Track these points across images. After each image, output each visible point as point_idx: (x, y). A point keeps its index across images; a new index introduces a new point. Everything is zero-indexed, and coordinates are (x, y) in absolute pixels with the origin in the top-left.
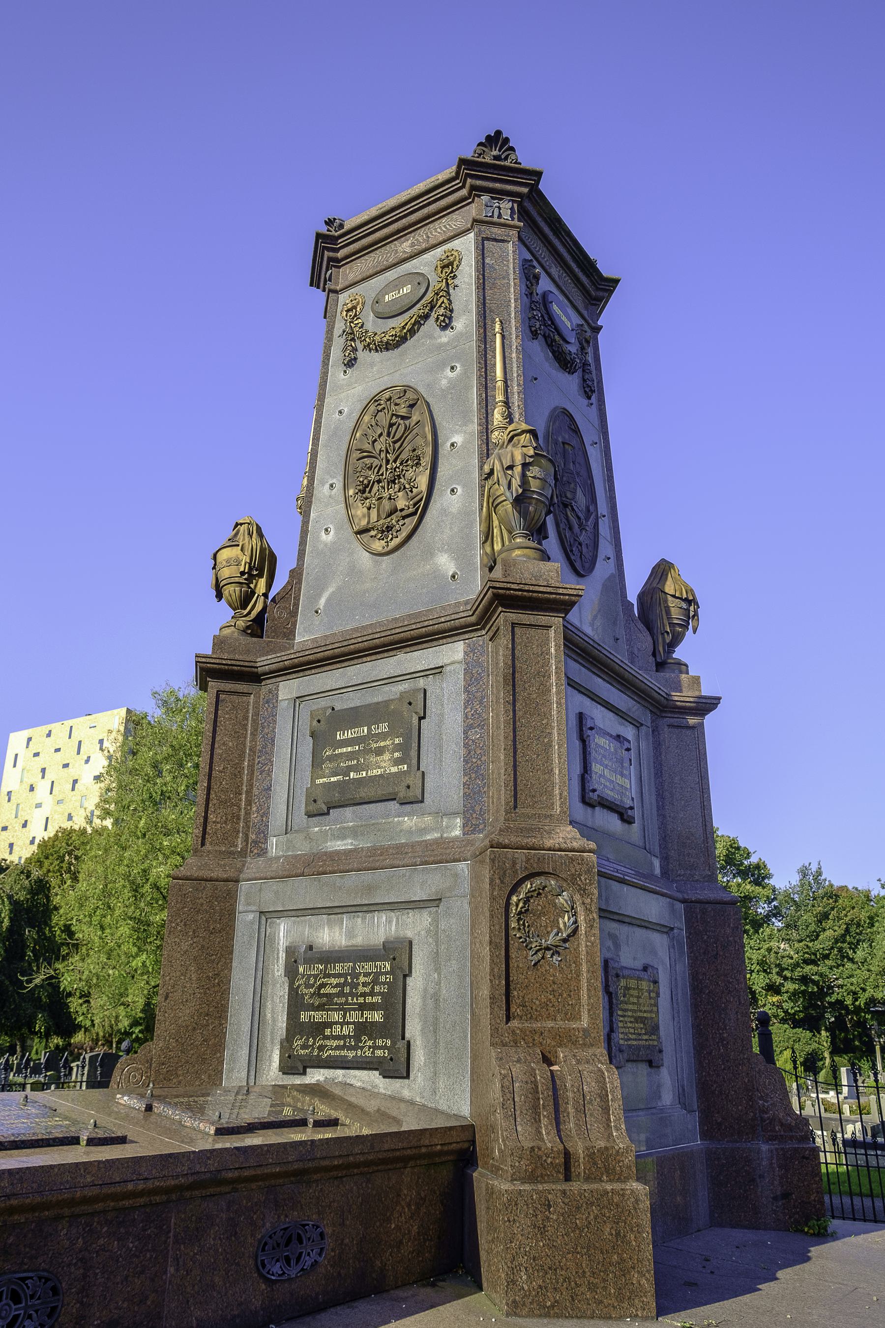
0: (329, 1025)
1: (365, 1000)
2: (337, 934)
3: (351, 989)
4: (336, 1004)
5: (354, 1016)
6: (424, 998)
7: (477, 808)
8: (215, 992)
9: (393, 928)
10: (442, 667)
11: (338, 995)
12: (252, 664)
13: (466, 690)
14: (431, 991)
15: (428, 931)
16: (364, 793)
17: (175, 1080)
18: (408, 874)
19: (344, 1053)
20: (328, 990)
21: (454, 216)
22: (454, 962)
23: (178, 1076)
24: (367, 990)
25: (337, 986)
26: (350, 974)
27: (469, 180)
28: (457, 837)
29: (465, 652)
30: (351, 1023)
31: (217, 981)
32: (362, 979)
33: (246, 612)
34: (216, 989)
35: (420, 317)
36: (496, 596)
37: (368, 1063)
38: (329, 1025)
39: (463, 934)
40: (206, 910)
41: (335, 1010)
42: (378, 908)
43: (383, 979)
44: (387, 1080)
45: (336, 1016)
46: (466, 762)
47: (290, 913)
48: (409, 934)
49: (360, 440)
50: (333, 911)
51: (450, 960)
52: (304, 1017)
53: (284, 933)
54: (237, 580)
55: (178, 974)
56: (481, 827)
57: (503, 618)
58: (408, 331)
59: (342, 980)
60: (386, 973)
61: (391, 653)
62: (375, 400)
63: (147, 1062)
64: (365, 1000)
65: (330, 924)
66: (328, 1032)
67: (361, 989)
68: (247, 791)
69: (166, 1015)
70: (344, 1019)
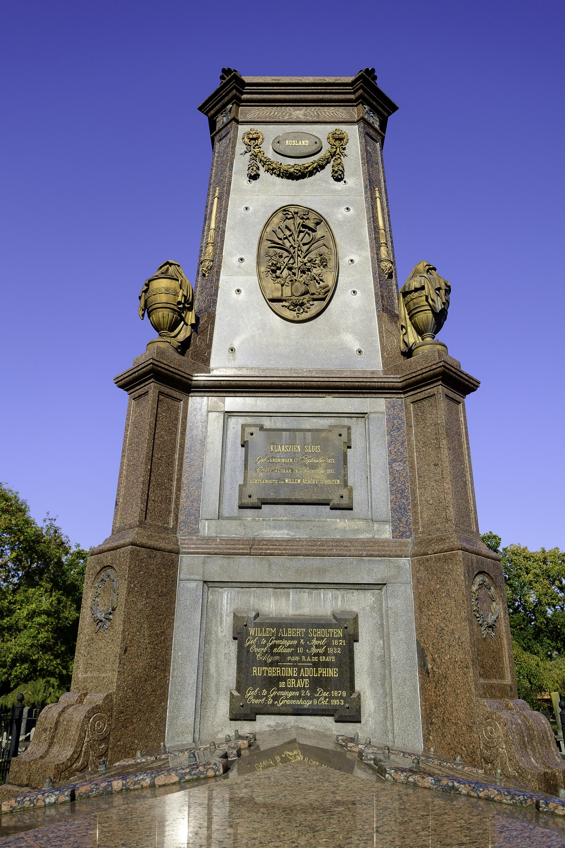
0: (285, 679)
1: (319, 659)
2: (284, 604)
3: (305, 650)
4: (290, 661)
5: (309, 672)
6: (371, 659)
7: (404, 520)
8: (162, 648)
9: (339, 603)
10: (366, 413)
11: (292, 654)
12: (189, 377)
13: (389, 433)
14: (378, 654)
15: (372, 608)
16: (306, 712)
17: (130, 728)
18: (355, 563)
19: (298, 702)
20: (280, 650)
21: (341, 109)
22: (402, 632)
23: (133, 723)
24: (321, 651)
25: (289, 647)
26: (303, 638)
27: (234, 91)
28: (386, 541)
29: (387, 407)
30: (305, 678)
31: (163, 638)
32: (315, 642)
33: (173, 334)
34: (163, 645)
35: (319, 165)
36: (443, 374)
37: (325, 710)
38: (285, 679)
39: (408, 611)
40: (156, 575)
41: (290, 666)
42: (325, 586)
43: (335, 642)
44: (339, 724)
45: (291, 672)
46: (392, 485)
47: (235, 585)
48: (355, 609)
49: (270, 234)
50: (278, 585)
51: (397, 630)
52: (257, 671)
53: (227, 602)
54: (172, 306)
55: (135, 629)
56: (407, 534)
57: (152, 387)
58: (310, 171)
59: (295, 642)
60: (339, 638)
61: (321, 395)
62: (284, 209)
63: (109, 711)
64: (319, 659)
65: (275, 595)
66: (282, 684)
67: (314, 650)
68: (177, 479)
69: (125, 667)
70: (299, 674)
